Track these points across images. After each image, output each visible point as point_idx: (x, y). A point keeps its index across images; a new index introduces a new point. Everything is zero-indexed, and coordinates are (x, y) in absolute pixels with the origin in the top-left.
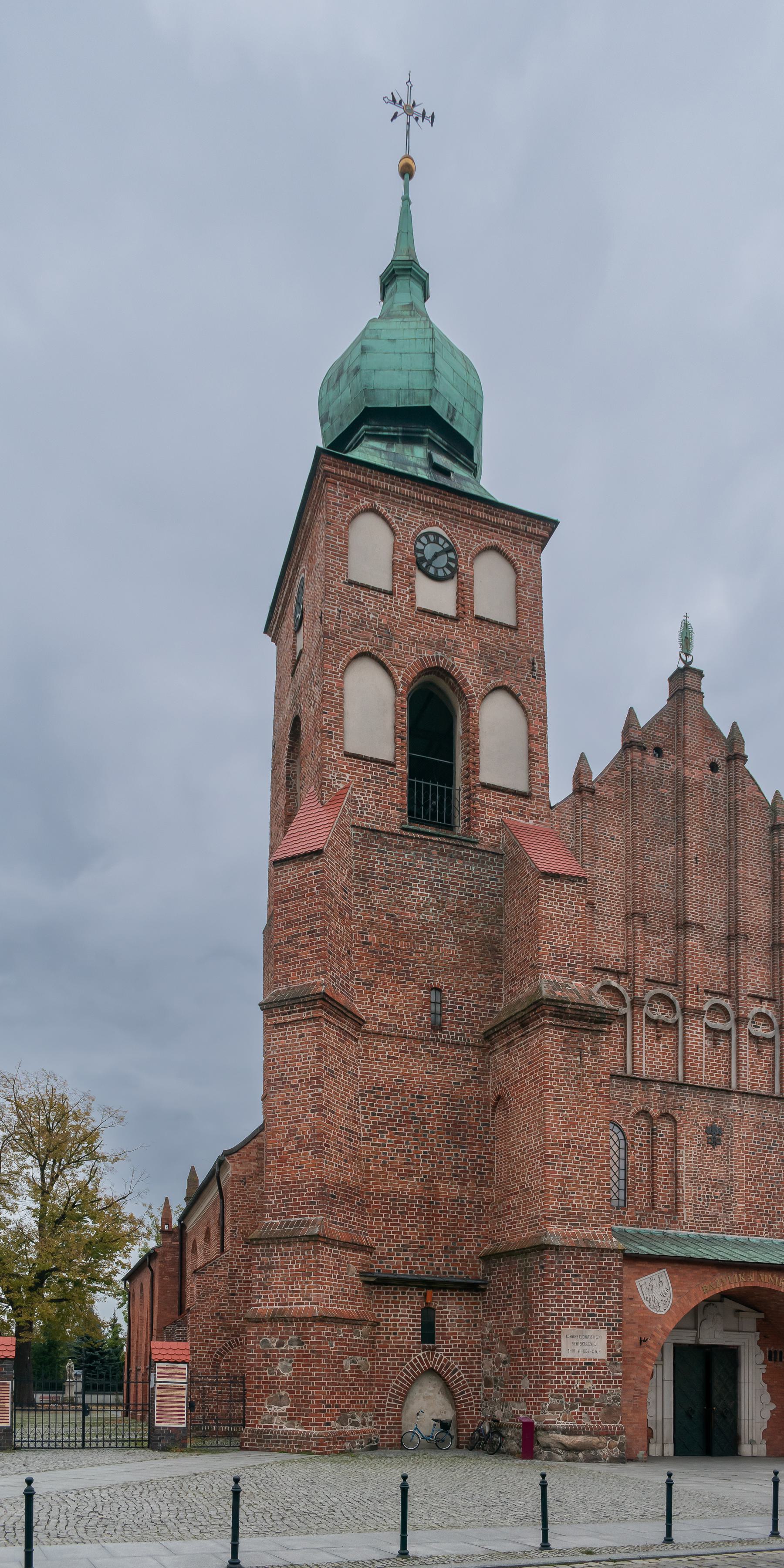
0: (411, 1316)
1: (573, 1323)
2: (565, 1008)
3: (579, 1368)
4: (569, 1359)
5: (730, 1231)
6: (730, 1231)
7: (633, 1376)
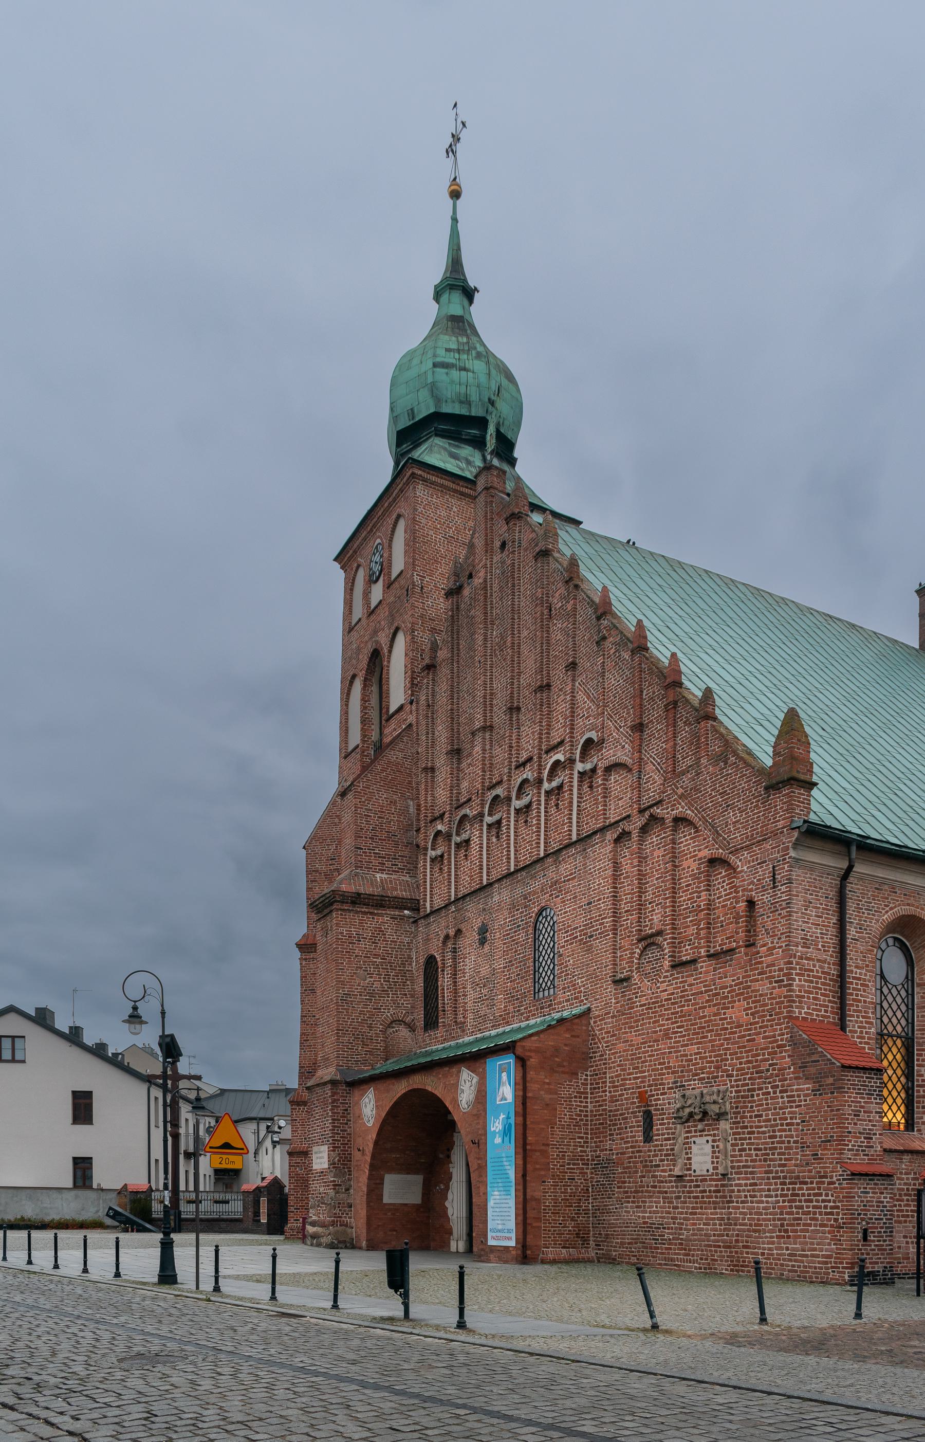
2: (317, 905)
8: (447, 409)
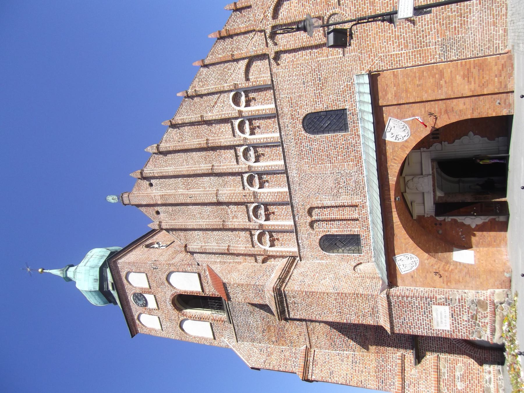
0: (433, 341)
1: (430, 323)
3: (455, 321)
4: (451, 326)
5: (362, 173)
6: (362, 173)
7: (457, 278)
8: (101, 264)
